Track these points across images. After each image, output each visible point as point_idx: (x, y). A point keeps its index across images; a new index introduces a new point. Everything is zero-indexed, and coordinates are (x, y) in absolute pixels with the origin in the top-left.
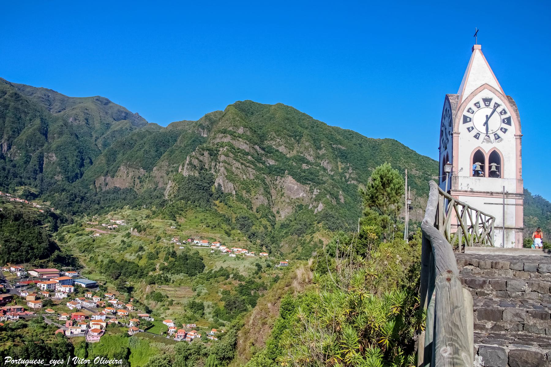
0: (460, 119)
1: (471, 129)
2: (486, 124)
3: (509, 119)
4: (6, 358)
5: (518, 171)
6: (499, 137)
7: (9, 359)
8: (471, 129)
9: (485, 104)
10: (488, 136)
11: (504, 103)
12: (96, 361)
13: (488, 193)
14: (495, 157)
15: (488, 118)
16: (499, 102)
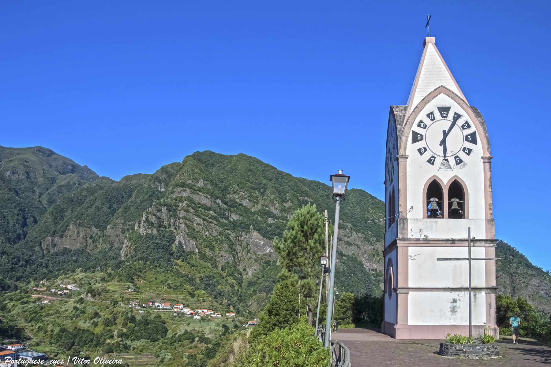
0: (407, 137)
1: (423, 150)
2: (443, 142)
3: (473, 135)
4: (6, 358)
5: (488, 207)
6: (461, 161)
7: (9, 359)
8: (423, 150)
9: (441, 114)
10: (447, 160)
11: (467, 112)
12: (96, 361)
13: (448, 240)
14: (457, 189)
15: (445, 134)
16: (461, 111)
